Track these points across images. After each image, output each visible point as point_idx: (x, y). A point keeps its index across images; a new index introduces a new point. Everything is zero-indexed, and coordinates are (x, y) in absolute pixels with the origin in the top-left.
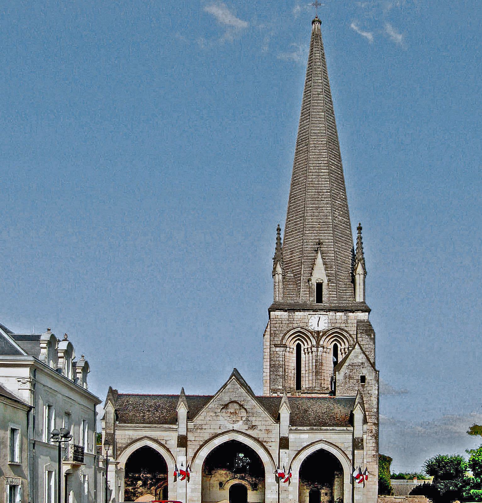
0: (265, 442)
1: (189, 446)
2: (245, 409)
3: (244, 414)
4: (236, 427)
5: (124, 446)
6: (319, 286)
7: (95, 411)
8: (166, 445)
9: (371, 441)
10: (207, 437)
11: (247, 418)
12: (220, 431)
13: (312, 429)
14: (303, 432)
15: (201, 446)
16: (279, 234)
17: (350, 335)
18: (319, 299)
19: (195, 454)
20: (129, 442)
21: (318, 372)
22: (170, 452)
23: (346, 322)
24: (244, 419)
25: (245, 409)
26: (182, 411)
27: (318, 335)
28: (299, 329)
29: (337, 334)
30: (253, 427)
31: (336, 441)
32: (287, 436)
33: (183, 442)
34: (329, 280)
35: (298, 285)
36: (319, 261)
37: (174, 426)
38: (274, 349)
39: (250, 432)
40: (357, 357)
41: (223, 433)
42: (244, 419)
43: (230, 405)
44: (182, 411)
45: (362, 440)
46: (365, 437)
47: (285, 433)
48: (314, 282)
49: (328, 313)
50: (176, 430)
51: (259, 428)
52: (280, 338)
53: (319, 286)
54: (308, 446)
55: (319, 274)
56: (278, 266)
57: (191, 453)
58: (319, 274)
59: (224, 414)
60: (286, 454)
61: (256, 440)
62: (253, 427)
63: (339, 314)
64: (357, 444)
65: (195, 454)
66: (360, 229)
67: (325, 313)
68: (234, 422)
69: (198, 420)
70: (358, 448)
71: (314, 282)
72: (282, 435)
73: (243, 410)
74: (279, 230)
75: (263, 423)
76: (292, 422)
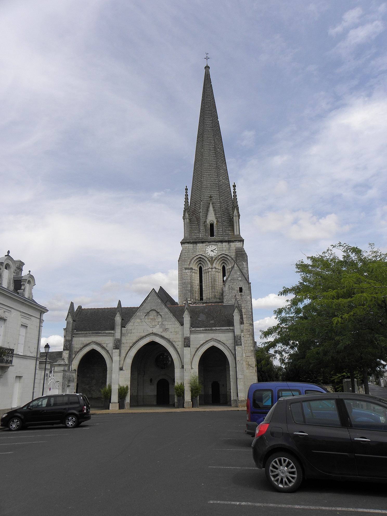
0: (174, 341)
1: (122, 349)
2: (161, 315)
3: (160, 319)
4: (155, 331)
5: (78, 350)
6: (212, 225)
7: (40, 319)
8: (107, 348)
9: (249, 339)
10: (135, 339)
11: (162, 323)
12: (143, 334)
13: (206, 330)
14: (200, 332)
15: (131, 347)
16: (186, 192)
17: (232, 259)
18: (212, 234)
19: (126, 355)
20: (81, 346)
21: (213, 287)
22: (109, 353)
23: (229, 249)
24: (160, 324)
25: (161, 315)
26: (118, 319)
27: (212, 260)
28: (200, 256)
29: (224, 259)
30: (166, 330)
31: (221, 339)
32: (189, 336)
33: (117, 345)
34: (217, 221)
35: (199, 225)
36: (211, 208)
37: (112, 332)
38: (184, 271)
39: (163, 334)
40: (236, 273)
41: (146, 336)
42: (160, 324)
43: (150, 313)
44: (118, 319)
45: (240, 337)
46: (242, 334)
47: (187, 334)
48: (208, 222)
49: (217, 244)
50: (113, 335)
51: (170, 330)
52: (188, 263)
53: (212, 225)
54: (204, 343)
55: (211, 218)
56: (186, 213)
57: (123, 355)
58: (211, 218)
59: (146, 320)
60: (23, 330)
61: (168, 341)
62: (166, 330)
63: (224, 244)
64: (237, 341)
65: (126, 355)
66: (234, 186)
67: (215, 244)
68: (154, 326)
69: (129, 326)
70: (238, 345)
71: (208, 222)
72: (185, 336)
73: (159, 316)
74: (186, 189)
75: (173, 326)
76: (193, 325)
